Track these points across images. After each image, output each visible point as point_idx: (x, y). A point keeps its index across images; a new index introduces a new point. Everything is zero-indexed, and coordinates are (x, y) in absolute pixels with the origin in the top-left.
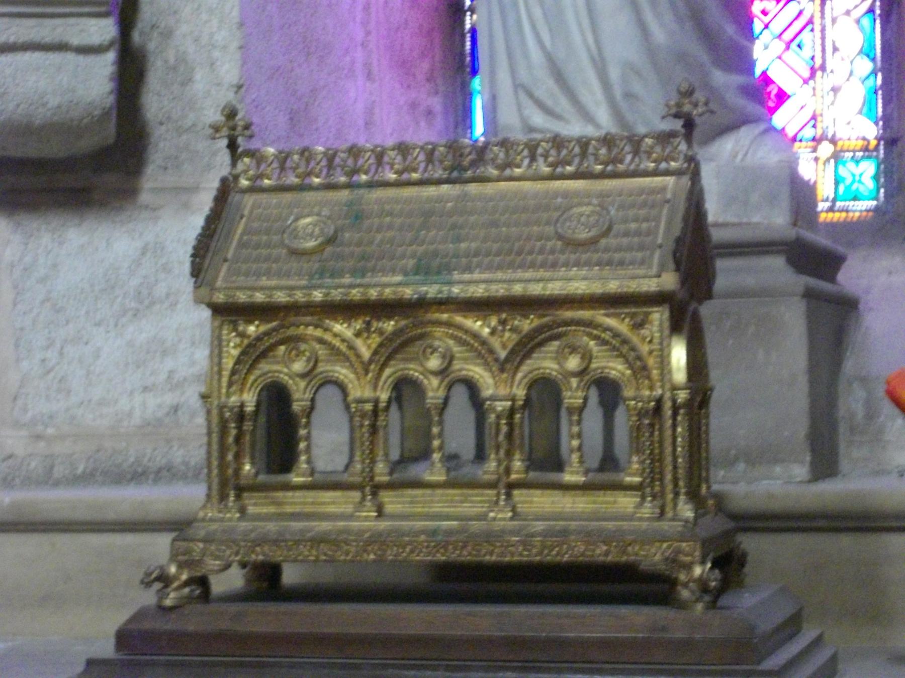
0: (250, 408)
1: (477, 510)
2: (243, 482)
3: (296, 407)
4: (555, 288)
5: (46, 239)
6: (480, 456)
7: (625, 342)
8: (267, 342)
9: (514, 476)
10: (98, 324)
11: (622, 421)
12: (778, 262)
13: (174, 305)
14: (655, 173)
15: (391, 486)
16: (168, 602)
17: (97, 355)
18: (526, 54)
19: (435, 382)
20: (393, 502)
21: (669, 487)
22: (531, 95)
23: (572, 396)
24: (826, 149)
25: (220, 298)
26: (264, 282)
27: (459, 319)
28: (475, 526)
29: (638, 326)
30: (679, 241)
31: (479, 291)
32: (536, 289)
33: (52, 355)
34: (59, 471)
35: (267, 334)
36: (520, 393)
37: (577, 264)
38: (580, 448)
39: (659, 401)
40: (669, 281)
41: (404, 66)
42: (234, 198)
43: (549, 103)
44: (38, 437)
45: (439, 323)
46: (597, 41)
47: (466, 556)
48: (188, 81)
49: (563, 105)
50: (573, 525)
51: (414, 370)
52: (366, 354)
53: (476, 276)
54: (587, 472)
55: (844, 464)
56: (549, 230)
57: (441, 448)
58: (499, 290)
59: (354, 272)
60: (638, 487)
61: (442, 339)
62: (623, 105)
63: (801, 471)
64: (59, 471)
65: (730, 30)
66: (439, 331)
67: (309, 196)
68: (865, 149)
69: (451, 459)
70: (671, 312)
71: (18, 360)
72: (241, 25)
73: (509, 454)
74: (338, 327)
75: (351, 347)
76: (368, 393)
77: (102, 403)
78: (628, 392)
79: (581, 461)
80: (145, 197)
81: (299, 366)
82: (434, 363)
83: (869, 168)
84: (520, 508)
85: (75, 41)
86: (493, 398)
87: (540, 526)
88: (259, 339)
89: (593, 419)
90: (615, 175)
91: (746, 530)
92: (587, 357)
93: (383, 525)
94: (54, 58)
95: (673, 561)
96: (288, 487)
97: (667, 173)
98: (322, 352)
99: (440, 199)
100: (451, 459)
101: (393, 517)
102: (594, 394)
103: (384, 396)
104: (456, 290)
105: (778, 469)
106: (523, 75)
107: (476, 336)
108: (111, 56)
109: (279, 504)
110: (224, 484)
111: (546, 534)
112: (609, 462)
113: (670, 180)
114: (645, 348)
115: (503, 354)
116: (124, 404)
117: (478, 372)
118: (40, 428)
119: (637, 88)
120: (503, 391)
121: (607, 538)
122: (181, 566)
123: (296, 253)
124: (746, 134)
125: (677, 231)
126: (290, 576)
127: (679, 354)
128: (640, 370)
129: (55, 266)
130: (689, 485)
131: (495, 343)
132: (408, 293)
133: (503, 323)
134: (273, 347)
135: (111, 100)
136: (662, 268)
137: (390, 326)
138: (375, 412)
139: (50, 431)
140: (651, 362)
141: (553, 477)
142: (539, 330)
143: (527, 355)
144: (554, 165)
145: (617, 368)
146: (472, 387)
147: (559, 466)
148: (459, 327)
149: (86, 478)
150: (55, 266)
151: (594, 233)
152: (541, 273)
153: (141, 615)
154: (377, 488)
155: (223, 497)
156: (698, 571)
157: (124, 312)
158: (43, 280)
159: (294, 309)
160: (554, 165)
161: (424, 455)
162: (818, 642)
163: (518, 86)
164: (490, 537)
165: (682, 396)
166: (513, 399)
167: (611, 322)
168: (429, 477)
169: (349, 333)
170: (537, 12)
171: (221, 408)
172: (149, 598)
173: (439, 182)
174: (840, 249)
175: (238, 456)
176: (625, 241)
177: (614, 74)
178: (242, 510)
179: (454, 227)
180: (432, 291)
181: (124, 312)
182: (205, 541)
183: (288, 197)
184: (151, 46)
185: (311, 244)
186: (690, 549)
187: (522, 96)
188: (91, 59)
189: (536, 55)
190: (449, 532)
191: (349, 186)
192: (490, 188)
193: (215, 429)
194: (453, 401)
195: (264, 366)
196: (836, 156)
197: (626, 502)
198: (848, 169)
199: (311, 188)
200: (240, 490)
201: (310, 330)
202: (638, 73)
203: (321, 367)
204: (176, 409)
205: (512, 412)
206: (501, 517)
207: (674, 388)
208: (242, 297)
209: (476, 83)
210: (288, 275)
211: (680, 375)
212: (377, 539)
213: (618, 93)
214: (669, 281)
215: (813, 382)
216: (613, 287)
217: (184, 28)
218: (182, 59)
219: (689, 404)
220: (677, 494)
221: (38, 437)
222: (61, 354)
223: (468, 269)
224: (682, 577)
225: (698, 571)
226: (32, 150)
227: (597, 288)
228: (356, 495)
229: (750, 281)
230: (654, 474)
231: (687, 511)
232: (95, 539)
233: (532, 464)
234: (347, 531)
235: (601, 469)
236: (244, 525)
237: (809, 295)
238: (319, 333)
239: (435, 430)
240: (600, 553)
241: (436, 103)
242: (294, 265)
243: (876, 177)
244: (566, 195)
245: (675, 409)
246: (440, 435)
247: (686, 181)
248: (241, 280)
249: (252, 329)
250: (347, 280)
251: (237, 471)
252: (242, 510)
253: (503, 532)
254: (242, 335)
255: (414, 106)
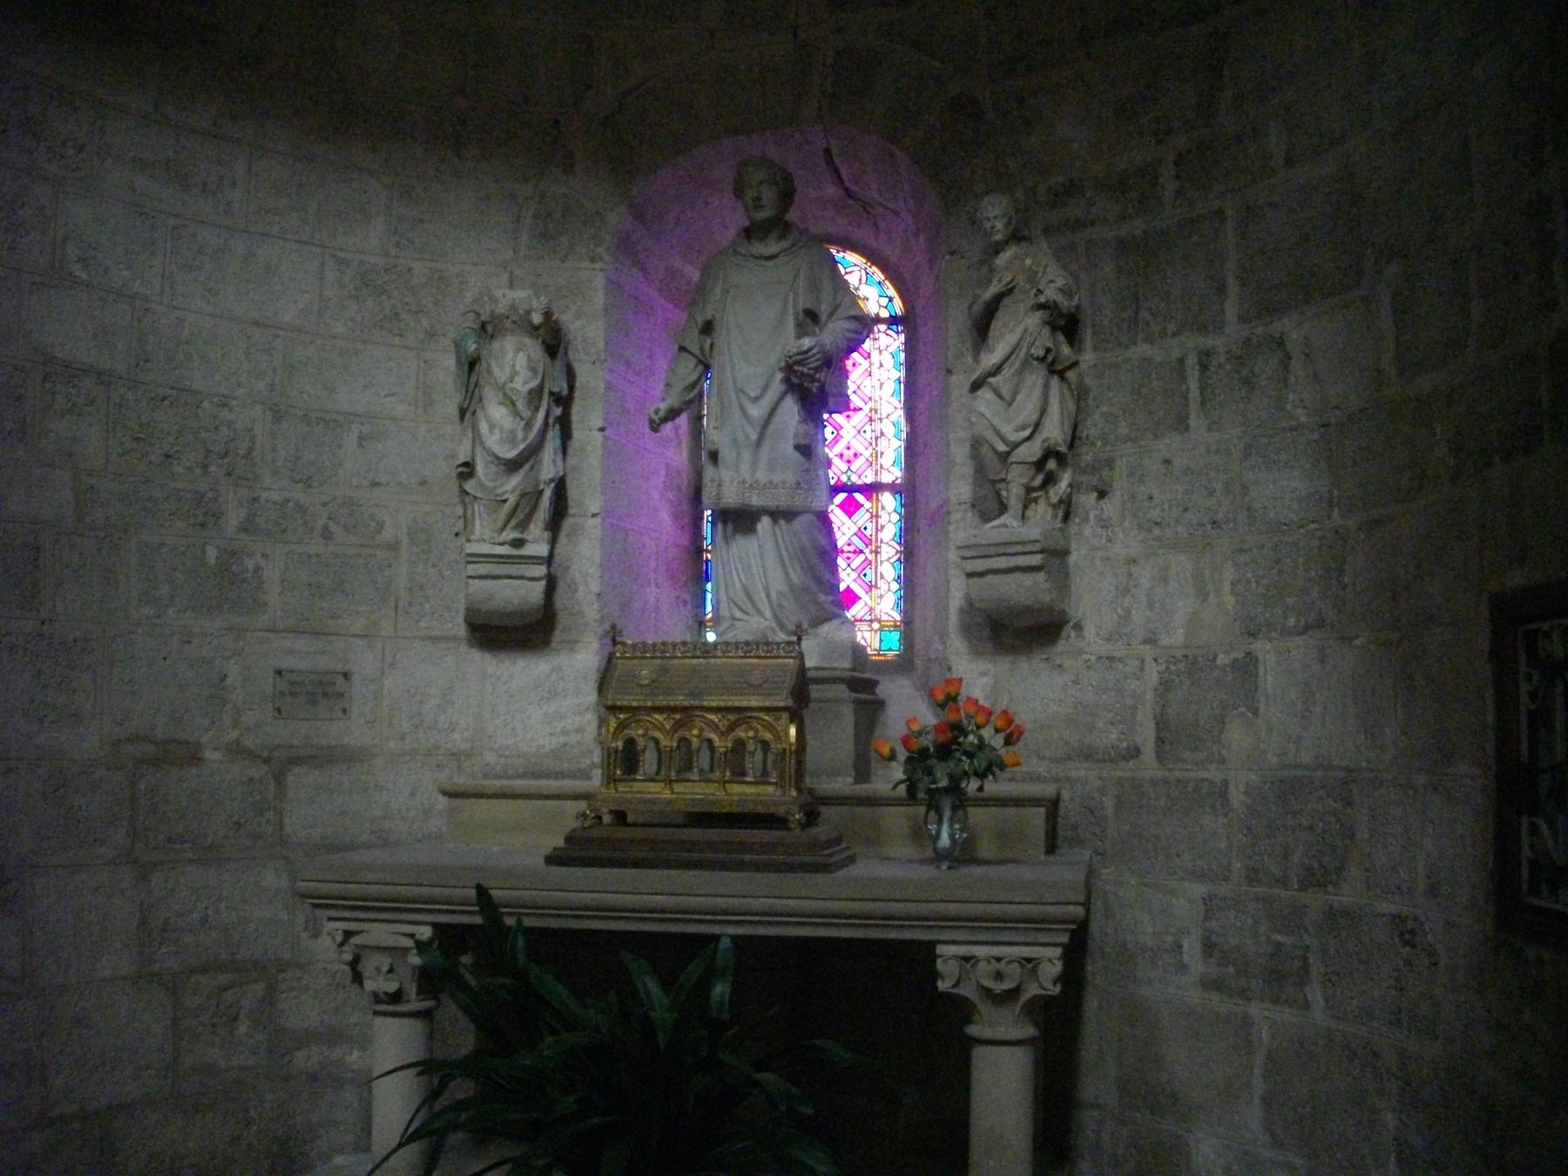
0: (620, 748)
1: (712, 791)
2: (617, 778)
3: (639, 748)
4: (745, 704)
5: (508, 664)
6: (712, 770)
7: (772, 725)
8: (627, 722)
9: (726, 778)
10: (530, 704)
11: (771, 758)
12: (843, 687)
13: (565, 697)
14: (785, 658)
15: (676, 781)
16: (586, 825)
17: (529, 718)
18: (733, 584)
19: (695, 740)
20: (678, 788)
21: (787, 784)
22: (735, 604)
23: (751, 747)
24: (876, 626)
25: (610, 703)
26: (627, 697)
27: (706, 715)
28: (711, 797)
29: (777, 719)
30: (793, 687)
31: (714, 704)
32: (737, 704)
33: (509, 717)
34: (510, 772)
35: (628, 719)
36: (730, 745)
37: (754, 694)
38: (753, 768)
39: (785, 750)
40: (790, 702)
41: (672, 577)
42: (614, 661)
43: (744, 608)
44: (501, 756)
45: (698, 716)
46: (767, 582)
47: (706, 809)
48: (576, 591)
49: (749, 608)
50: (750, 798)
51: (687, 734)
52: (668, 727)
53: (714, 698)
54: (755, 777)
55: (874, 778)
56: (743, 680)
57: (697, 767)
58: (722, 704)
59: (663, 694)
60: (776, 783)
61: (698, 723)
62: (778, 612)
63: (850, 780)
64: (510, 772)
65: (827, 576)
66: (698, 719)
67: (646, 662)
68: (895, 626)
69: (701, 771)
70: (1063, 334)
71: (492, 719)
72: (601, 565)
73: (724, 769)
74: (657, 716)
75: (662, 725)
76: (668, 743)
77: (532, 740)
78: (772, 746)
79: (753, 773)
80: (554, 645)
81: (640, 732)
82: (695, 732)
83: (896, 636)
84: (729, 791)
85: (528, 575)
86: (719, 747)
87: (736, 798)
88: (624, 720)
89: (759, 757)
90: (770, 658)
91: (823, 804)
92: (757, 731)
93: (674, 796)
94: (518, 582)
95: (788, 812)
96: (635, 780)
97: (791, 658)
98: (650, 726)
99: (699, 665)
100: (701, 771)
101: (676, 793)
102: (759, 746)
103: (675, 745)
104: (705, 703)
105: (840, 779)
106: (731, 594)
107: (712, 722)
108: (544, 582)
109: (631, 787)
110: (609, 778)
111: (740, 800)
112: (765, 773)
113: (791, 661)
114: (779, 729)
115: (723, 729)
116: (541, 741)
117: (712, 736)
118: (501, 752)
119: (785, 603)
120: (723, 744)
121: (762, 802)
122: (591, 811)
123: (639, 685)
124: (835, 623)
125: (793, 684)
126: (630, 819)
127: (793, 731)
128: (778, 738)
129: (511, 676)
130: (796, 782)
131: (720, 724)
132: (686, 703)
133: (723, 717)
134: (630, 723)
135: (543, 602)
136: (787, 698)
137: (678, 716)
138: (672, 750)
139: (507, 753)
140: (782, 734)
141: (741, 779)
142: (738, 720)
143: (733, 730)
144: (746, 652)
145: (768, 736)
146: (710, 741)
147: (744, 774)
148: (706, 718)
149: (523, 776)
150: (511, 676)
151: (761, 681)
152: (740, 698)
153: (574, 830)
154: (671, 781)
155: (609, 783)
156: (797, 816)
157: (543, 698)
158: (506, 683)
159: (638, 708)
160: (746, 652)
161: (690, 768)
162: (848, 848)
163: (729, 598)
164: (717, 802)
165: (794, 748)
166: (726, 747)
167: (766, 718)
168: (692, 778)
169: (661, 719)
170: (739, 566)
171: (608, 748)
172: (578, 824)
173: (699, 658)
174: (875, 677)
175: (615, 767)
176: (774, 685)
177: (774, 596)
178: (616, 790)
179: (705, 677)
180: (696, 703)
181: (543, 698)
182: (602, 801)
183: (636, 661)
184: (559, 574)
185: (646, 682)
186: (795, 808)
187: (732, 605)
188: (534, 583)
189: (738, 584)
190: (701, 800)
191: (662, 658)
192: (719, 661)
193: (606, 755)
194: (703, 749)
195: (626, 731)
196: (881, 630)
197: (770, 789)
198: (887, 634)
199: (646, 658)
200: (615, 781)
201: (646, 718)
202: (785, 596)
203: (649, 733)
204: (565, 744)
205: (726, 754)
206: (720, 794)
207: (791, 744)
208: (619, 703)
209: (709, 586)
210: (636, 695)
211: (793, 740)
212: (670, 802)
213: (775, 603)
214: (790, 702)
215: (857, 743)
216: (767, 704)
217: (574, 567)
218: (573, 581)
219: (797, 752)
220: (790, 786)
221: (501, 756)
222: (513, 717)
223: (710, 694)
224: (792, 819)
225: (797, 816)
226: (506, 622)
227: (761, 704)
228: (662, 785)
229: (829, 695)
230: (781, 777)
231: (794, 793)
232: (539, 803)
233: (734, 773)
234: (659, 799)
235: (762, 775)
236: (618, 795)
237: (856, 702)
238: (649, 718)
239: (695, 759)
240: (760, 809)
241: (687, 597)
242: (639, 691)
243: (899, 640)
244: (749, 664)
245: (791, 753)
246: (697, 761)
247: (797, 661)
248: (618, 697)
249: (622, 716)
250: (661, 698)
251: (615, 773)
252: (616, 790)
253: (722, 800)
254: (618, 718)
255: (678, 597)
